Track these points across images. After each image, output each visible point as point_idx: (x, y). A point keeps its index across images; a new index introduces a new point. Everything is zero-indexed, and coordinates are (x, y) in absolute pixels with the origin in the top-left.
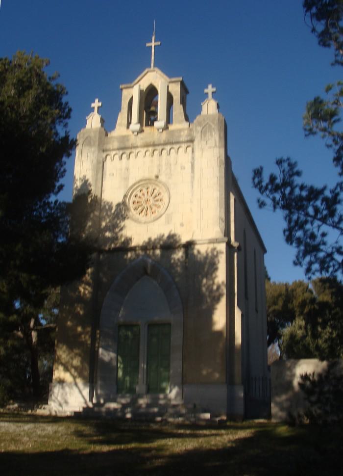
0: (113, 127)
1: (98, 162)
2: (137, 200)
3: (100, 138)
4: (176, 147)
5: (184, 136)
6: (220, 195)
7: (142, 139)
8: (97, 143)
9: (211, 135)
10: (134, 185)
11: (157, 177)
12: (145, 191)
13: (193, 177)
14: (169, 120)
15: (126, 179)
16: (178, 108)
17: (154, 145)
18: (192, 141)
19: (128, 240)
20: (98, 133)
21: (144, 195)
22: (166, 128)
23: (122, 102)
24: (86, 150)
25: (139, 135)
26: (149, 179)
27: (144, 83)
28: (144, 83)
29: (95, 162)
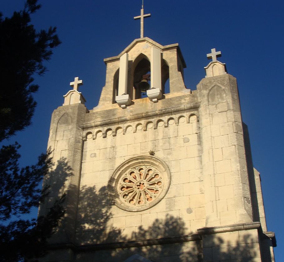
0: (96, 103)
1: (77, 141)
2: (127, 184)
3: (79, 115)
4: (176, 116)
5: (185, 103)
6: (242, 167)
7: (131, 112)
8: (75, 120)
9: (222, 98)
10: (123, 165)
11: (152, 153)
12: (136, 172)
13: (201, 151)
14: (165, 88)
15: (112, 159)
16: (175, 76)
17: (147, 117)
18: (196, 108)
19: (116, 233)
20: (77, 109)
21: (135, 178)
22: (161, 97)
23: (107, 75)
24: (62, 128)
25: (128, 107)
26: (142, 158)
27: (133, 53)
28: (133, 53)
29: (72, 140)
